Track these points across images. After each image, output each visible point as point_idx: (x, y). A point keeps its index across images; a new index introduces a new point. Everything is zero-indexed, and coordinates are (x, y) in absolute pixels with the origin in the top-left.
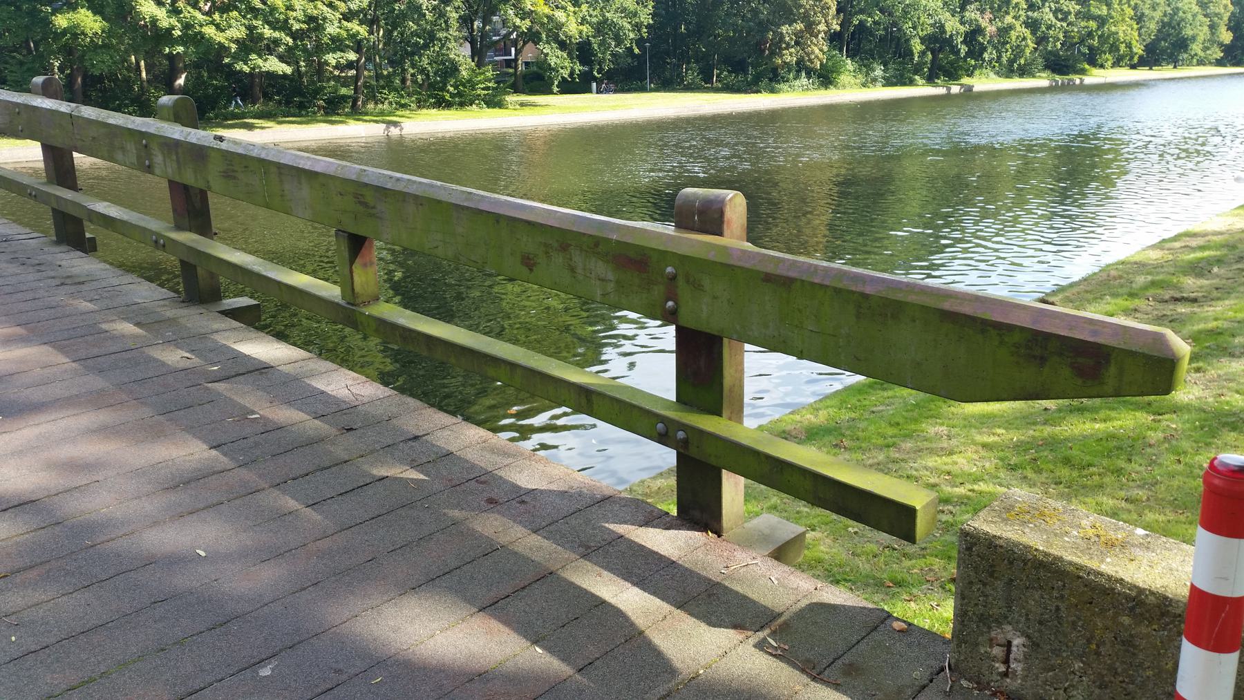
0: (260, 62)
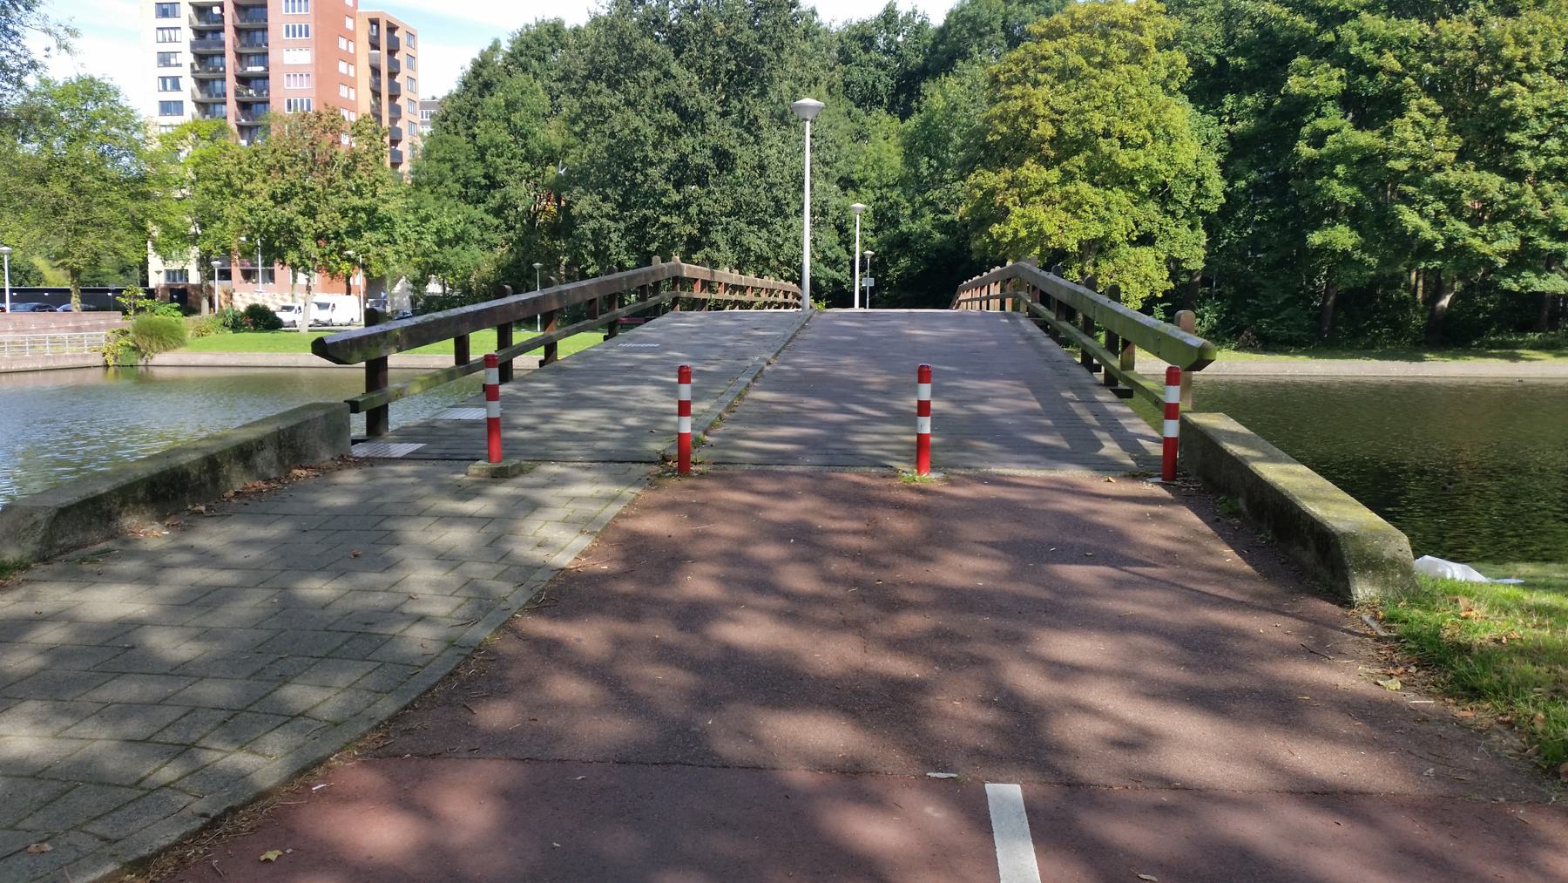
0: (1535, 281)
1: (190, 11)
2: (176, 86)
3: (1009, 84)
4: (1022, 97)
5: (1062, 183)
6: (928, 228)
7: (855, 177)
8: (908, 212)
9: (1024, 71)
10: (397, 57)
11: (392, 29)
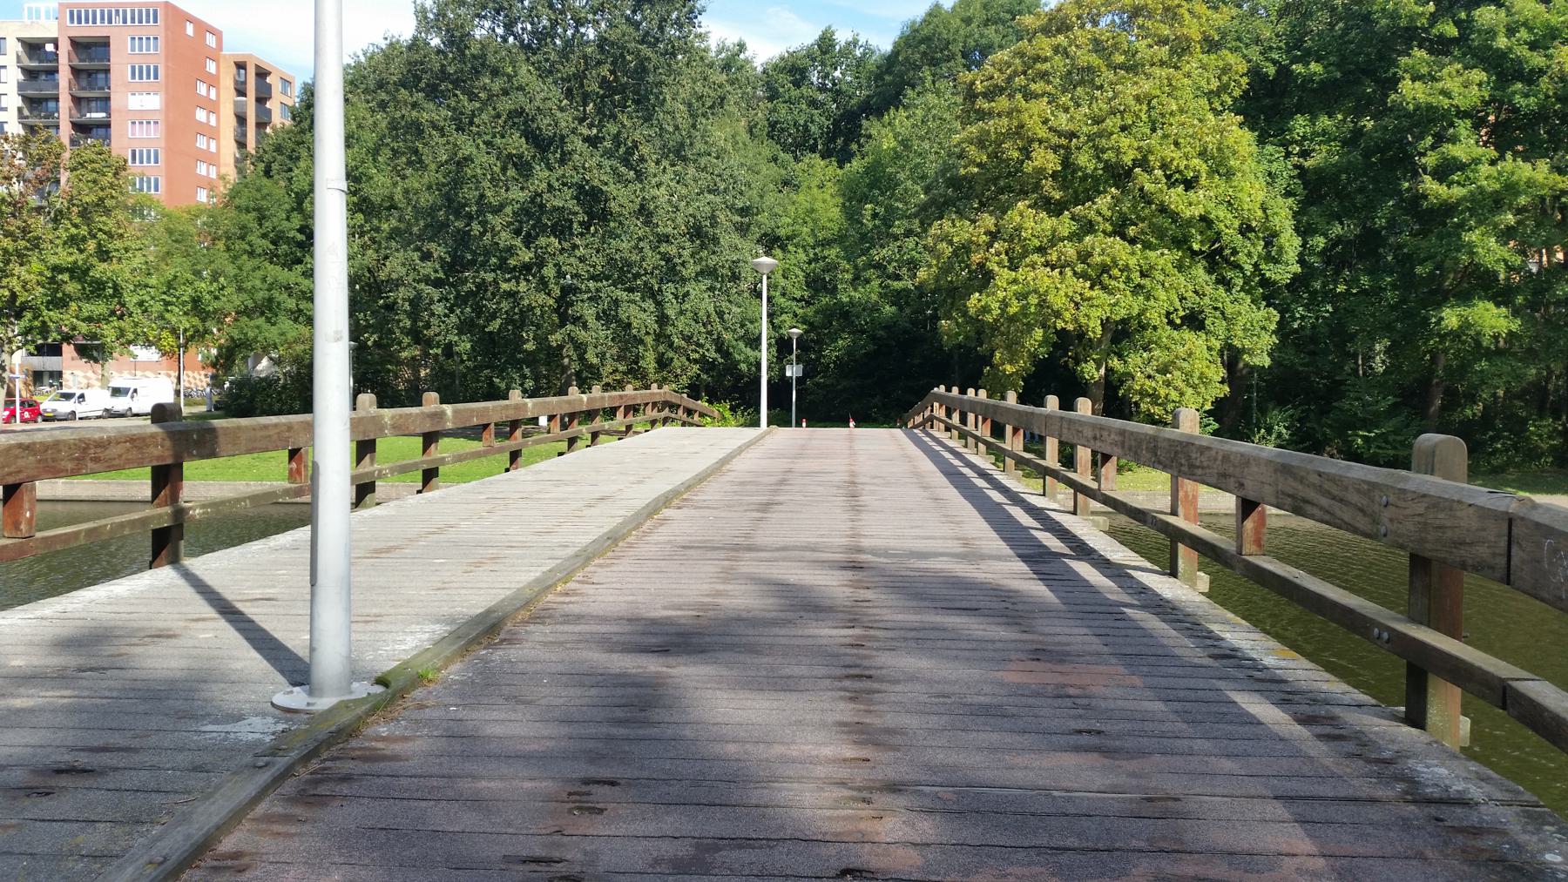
1: (19, 47)
3: (990, 95)
4: (1009, 114)
5: (1076, 237)
6: (874, 297)
7: (782, 232)
8: (848, 276)
9: (1009, 79)
10: (268, 105)
11: (262, 74)
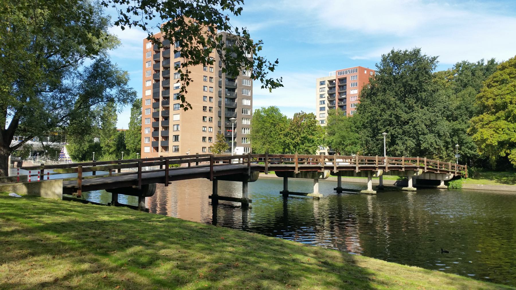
2: (324, 103)
